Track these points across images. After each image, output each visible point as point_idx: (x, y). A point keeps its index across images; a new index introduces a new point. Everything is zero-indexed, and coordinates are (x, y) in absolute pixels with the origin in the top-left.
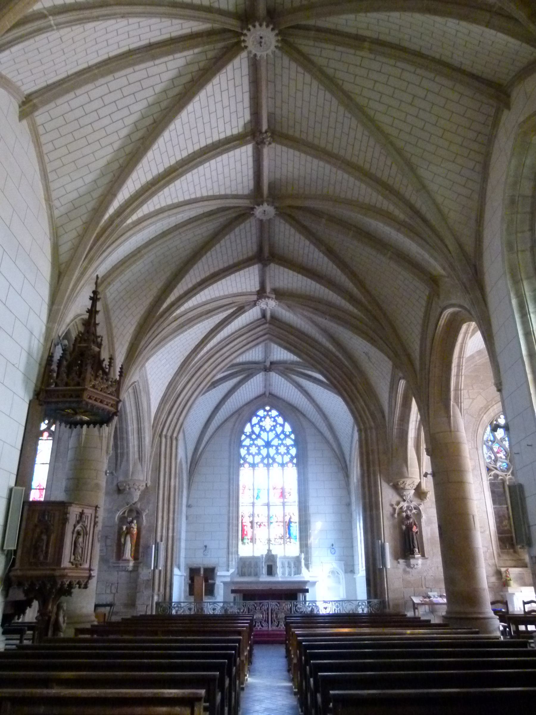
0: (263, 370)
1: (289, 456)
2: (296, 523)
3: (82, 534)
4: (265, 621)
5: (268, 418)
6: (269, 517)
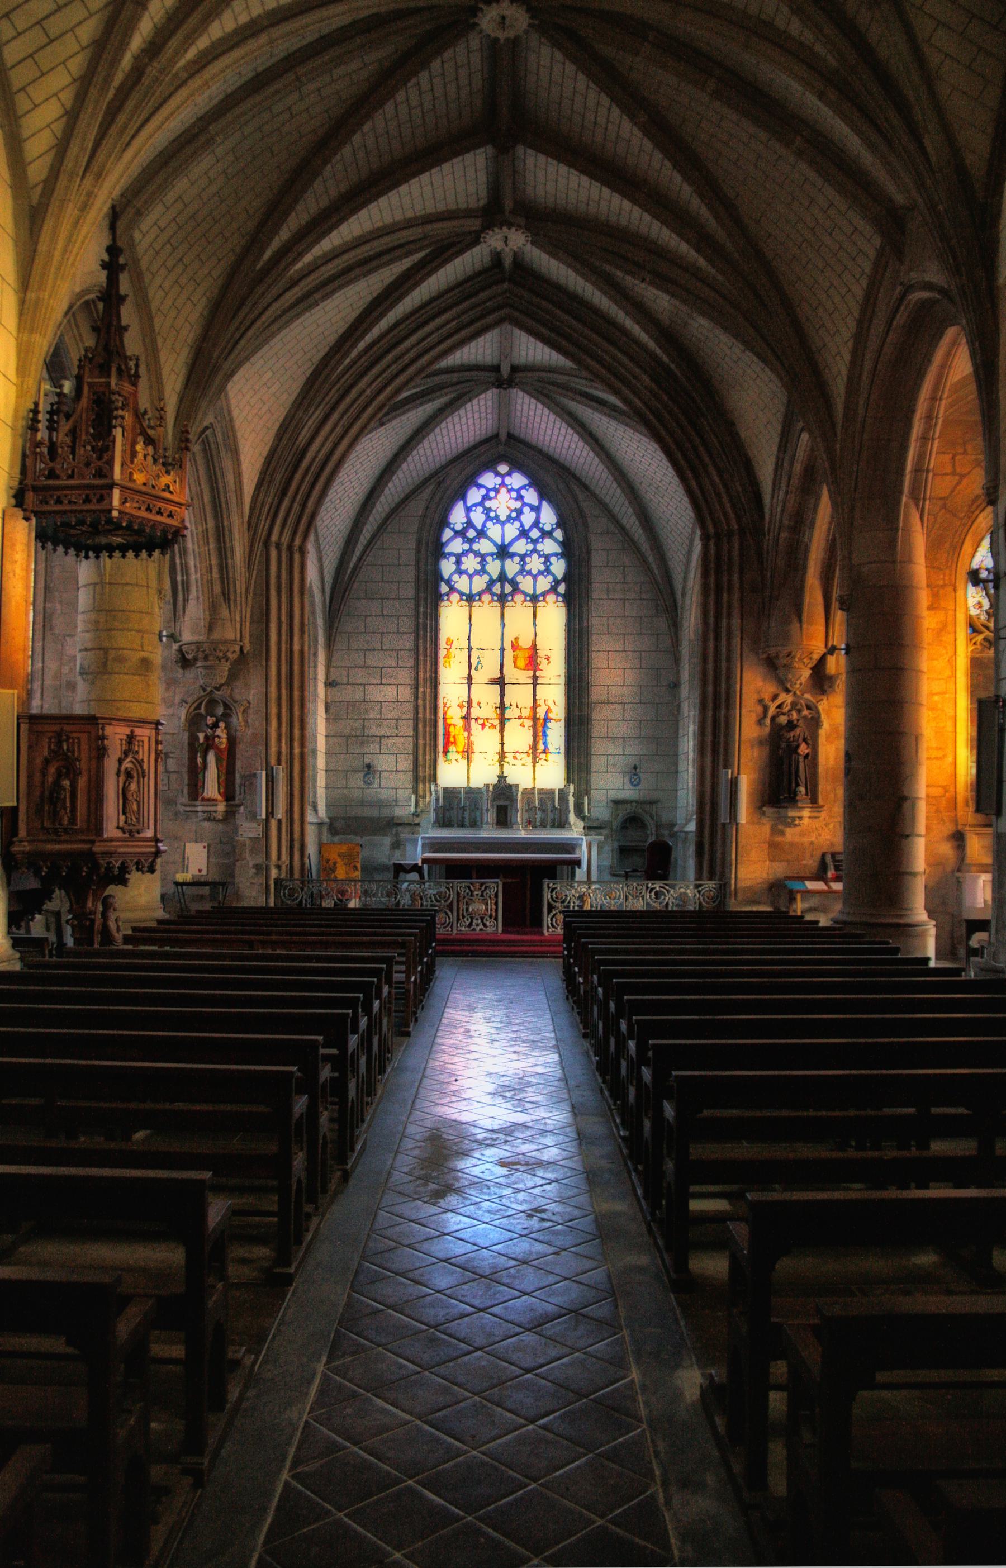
0: (493, 384)
1: (550, 578)
2: (559, 720)
3: (135, 775)
4: (491, 917)
5: (503, 490)
6: (502, 707)
